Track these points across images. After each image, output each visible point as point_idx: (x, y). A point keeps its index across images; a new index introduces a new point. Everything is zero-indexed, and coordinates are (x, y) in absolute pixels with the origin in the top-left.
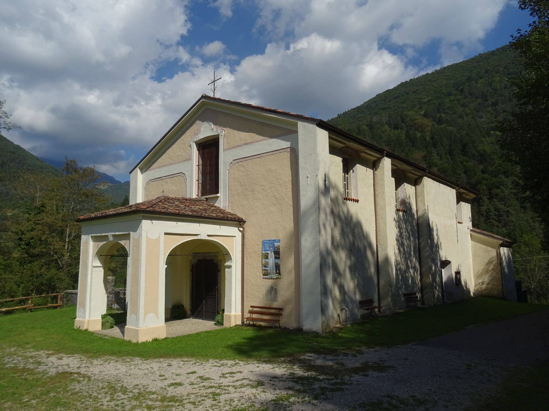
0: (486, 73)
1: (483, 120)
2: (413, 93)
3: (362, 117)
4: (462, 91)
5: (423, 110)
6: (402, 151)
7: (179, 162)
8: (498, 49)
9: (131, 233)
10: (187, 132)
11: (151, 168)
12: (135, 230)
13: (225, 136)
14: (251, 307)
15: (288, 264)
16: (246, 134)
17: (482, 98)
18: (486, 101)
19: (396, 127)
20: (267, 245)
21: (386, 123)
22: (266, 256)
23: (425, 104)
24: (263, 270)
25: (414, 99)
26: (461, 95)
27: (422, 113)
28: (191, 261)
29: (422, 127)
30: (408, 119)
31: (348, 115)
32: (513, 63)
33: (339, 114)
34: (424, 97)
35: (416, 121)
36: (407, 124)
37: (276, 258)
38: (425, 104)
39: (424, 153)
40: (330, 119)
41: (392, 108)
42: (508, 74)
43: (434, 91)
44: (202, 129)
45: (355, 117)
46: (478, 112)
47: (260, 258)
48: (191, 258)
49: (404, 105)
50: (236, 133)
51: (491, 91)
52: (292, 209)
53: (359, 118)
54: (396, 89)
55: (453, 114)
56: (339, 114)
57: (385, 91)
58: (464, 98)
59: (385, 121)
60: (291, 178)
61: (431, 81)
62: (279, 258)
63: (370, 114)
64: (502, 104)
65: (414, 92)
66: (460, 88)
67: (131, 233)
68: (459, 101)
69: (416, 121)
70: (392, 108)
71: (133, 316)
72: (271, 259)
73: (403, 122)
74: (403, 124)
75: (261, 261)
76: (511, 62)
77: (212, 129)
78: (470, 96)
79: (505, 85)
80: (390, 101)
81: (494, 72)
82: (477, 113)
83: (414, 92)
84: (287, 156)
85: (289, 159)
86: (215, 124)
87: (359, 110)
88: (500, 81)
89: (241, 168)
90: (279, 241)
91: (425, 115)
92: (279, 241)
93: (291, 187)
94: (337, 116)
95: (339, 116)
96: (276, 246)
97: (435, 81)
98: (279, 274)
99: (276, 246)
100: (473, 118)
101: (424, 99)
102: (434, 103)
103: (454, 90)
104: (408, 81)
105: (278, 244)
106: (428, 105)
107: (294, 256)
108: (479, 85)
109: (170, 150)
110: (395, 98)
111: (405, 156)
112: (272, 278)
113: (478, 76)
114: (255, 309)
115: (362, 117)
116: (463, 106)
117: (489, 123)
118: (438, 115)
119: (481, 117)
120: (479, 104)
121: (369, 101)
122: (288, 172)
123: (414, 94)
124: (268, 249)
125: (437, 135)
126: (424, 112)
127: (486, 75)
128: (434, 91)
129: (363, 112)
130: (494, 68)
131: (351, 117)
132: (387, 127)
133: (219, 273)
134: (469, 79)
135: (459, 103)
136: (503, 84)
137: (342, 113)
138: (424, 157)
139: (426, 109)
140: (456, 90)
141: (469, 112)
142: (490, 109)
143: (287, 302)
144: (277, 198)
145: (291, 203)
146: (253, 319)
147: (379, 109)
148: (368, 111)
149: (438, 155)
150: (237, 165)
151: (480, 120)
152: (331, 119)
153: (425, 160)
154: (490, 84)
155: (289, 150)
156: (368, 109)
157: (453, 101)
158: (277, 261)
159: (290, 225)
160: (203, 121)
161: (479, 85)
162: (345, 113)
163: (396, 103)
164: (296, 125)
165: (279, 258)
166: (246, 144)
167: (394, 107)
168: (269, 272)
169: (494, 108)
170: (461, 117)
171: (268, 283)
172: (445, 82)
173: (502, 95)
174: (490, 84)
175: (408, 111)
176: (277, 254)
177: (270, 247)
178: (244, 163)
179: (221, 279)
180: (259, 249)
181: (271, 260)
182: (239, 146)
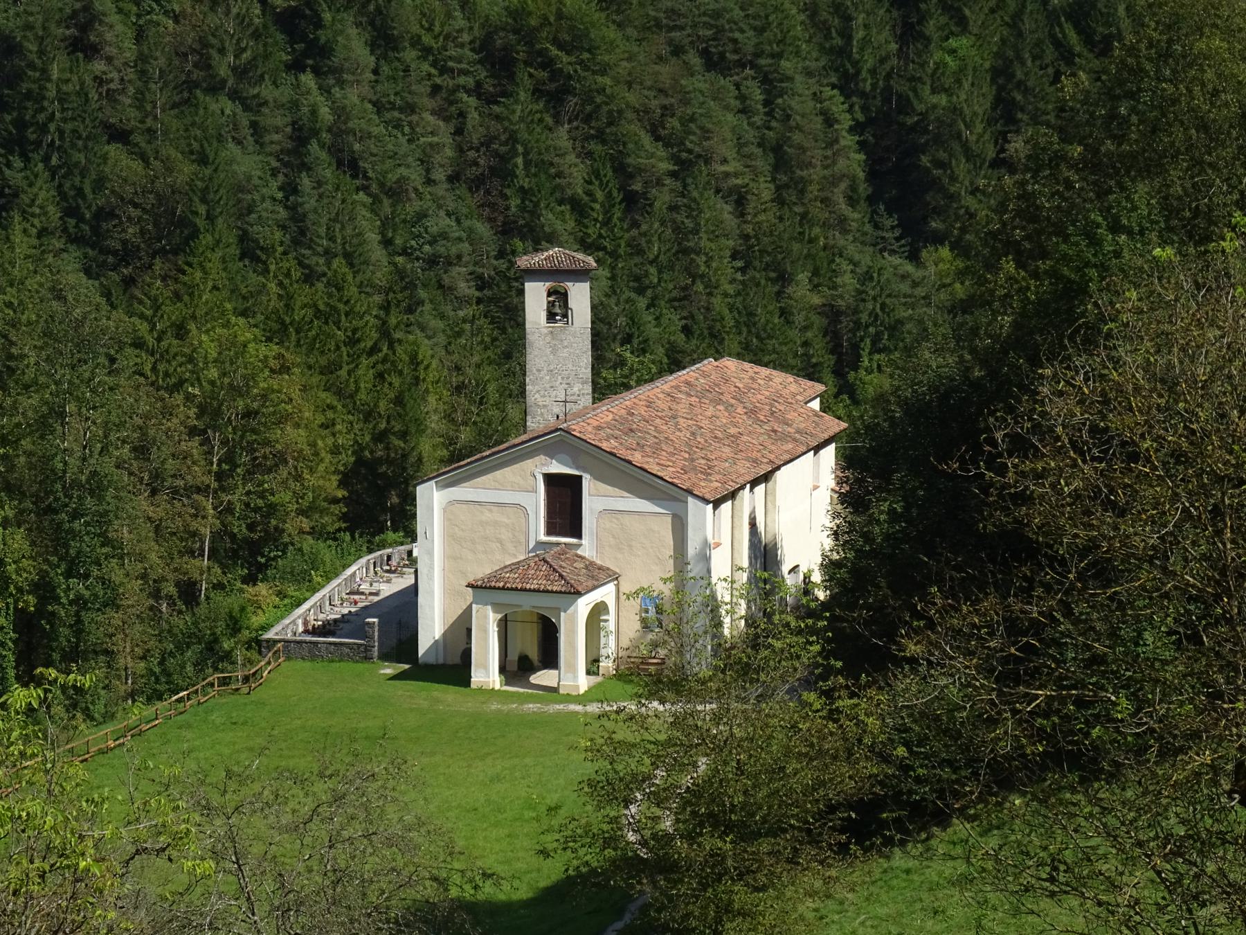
71: (570, 675)
159: (669, 569)
178: (619, 516)
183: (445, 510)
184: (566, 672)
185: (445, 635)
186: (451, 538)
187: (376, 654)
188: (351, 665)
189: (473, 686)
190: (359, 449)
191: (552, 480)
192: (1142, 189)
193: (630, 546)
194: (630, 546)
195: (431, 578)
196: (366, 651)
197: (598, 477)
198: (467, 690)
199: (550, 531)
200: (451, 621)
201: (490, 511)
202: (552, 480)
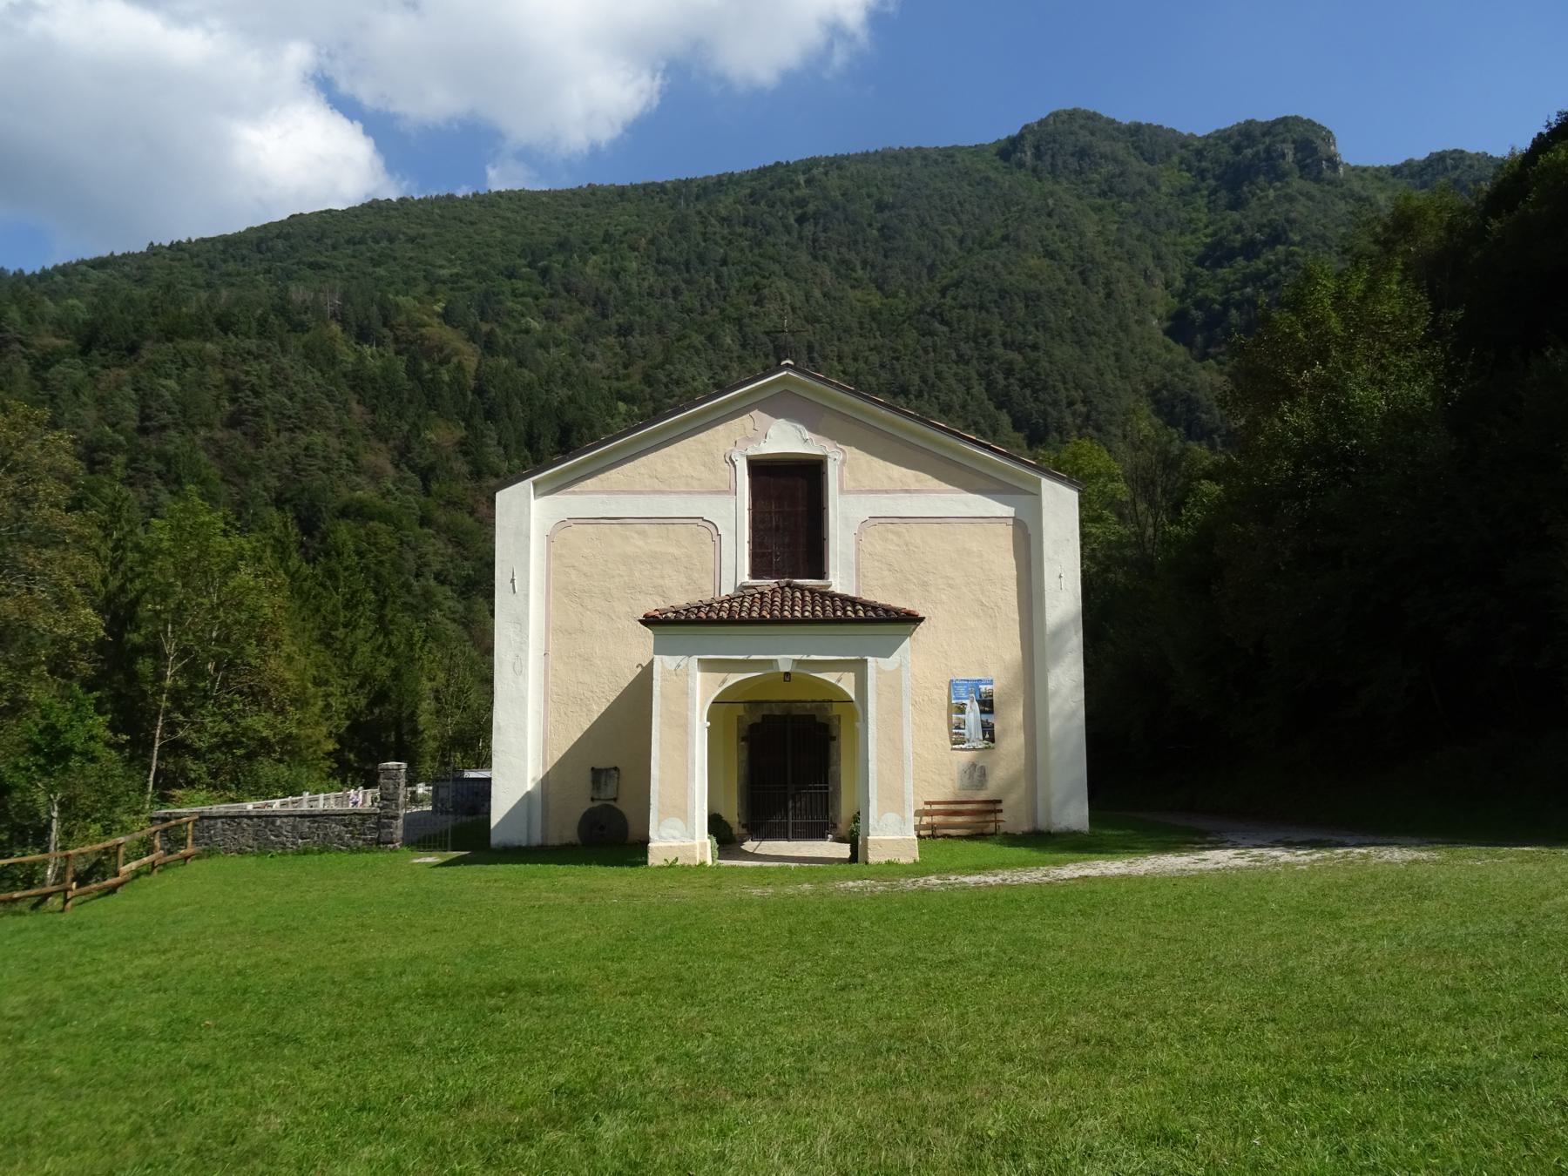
0: (604, 241)
1: (596, 365)
2: (407, 241)
3: (239, 274)
4: (545, 273)
5: (439, 300)
6: (400, 416)
7: (689, 493)
8: (635, 187)
9: (870, 659)
10: (720, 427)
11: (576, 488)
12: (887, 653)
13: (843, 462)
14: (926, 803)
15: (1011, 720)
16: (904, 470)
17: (594, 305)
18: (605, 316)
19: (363, 335)
20: (962, 691)
21: (334, 315)
22: (961, 709)
23: (444, 282)
24: (951, 734)
25: (411, 258)
26: (544, 285)
27: (438, 308)
28: (740, 719)
29: (441, 350)
30: (402, 318)
31: (187, 256)
32: (670, 237)
33: (156, 244)
34: (440, 262)
35: (424, 331)
36: (399, 333)
37: (982, 712)
38: (444, 282)
39: (460, 433)
40: (118, 253)
41: (341, 272)
42: (658, 261)
43: (469, 254)
44: (771, 433)
45: (212, 267)
46: (585, 342)
47: (945, 714)
48: (740, 710)
49: (381, 271)
50: (878, 463)
51: (618, 293)
52: (1017, 627)
53: (229, 275)
54: (356, 216)
55: (521, 332)
56: (156, 244)
57: (321, 212)
58: (551, 296)
59: (329, 309)
60: (1015, 572)
61: (461, 221)
62: (991, 712)
63: (268, 271)
64: (642, 335)
65: (412, 240)
66: (540, 264)
67: (870, 659)
68: (537, 298)
69: (424, 331)
70: (341, 272)
72: (972, 715)
73: (385, 325)
74: (386, 331)
75: (945, 716)
76: (666, 231)
77: (806, 441)
78: (565, 294)
79: (651, 287)
80: (334, 248)
81: (625, 245)
82: (582, 346)
83: (412, 240)
84: (1004, 538)
85: (1011, 538)
86: (812, 429)
87: (229, 245)
88: (639, 273)
89: (891, 536)
90: (991, 682)
91: (447, 317)
92: (991, 682)
93: (1015, 588)
94: (145, 250)
95: (154, 251)
96: (983, 690)
97: (472, 223)
98: (992, 740)
99: (983, 690)
100: (572, 355)
101: (441, 267)
102: (468, 288)
103: (525, 266)
104: (394, 200)
105: (989, 687)
106: (452, 289)
107: (1021, 710)
108: (588, 270)
109: (651, 456)
110: (350, 241)
111: (410, 431)
112: (974, 749)
113: (586, 243)
114: (935, 807)
115: (239, 274)
116: (548, 315)
117: (608, 378)
118: (485, 328)
119: (592, 358)
120: (588, 320)
121: (265, 226)
122: (1006, 566)
123: (410, 246)
124: (964, 695)
125: (494, 387)
126: (445, 308)
127: (606, 246)
128: (469, 254)
129: (243, 260)
130: (625, 233)
131: (199, 265)
132: (336, 328)
133: (834, 744)
134: (563, 245)
135: (537, 306)
136: (646, 284)
137: (167, 243)
138: (462, 443)
139: (450, 302)
140: (530, 265)
141: (563, 336)
142: (612, 340)
143: (1010, 786)
144: (982, 604)
145: (1017, 617)
146: (932, 827)
147: (298, 264)
148: (261, 260)
149: (499, 443)
150: (880, 527)
151: (588, 364)
152: (124, 256)
153: (466, 454)
154: (616, 275)
155: (1011, 522)
156: (260, 252)
157: (523, 295)
158: (985, 717)
159: (1011, 651)
160: (777, 416)
161: (588, 270)
162: (177, 247)
163: (354, 257)
164: (1039, 483)
165: (991, 712)
166: (907, 491)
167: (347, 270)
168: (967, 736)
169: (622, 339)
170: (543, 345)
171: (965, 757)
172: (499, 234)
173: (641, 312)
174: (616, 275)
175: (397, 293)
176: (987, 705)
177: (969, 692)
178: (902, 528)
179: (839, 755)
180: (941, 696)
181: (973, 715)
182: (887, 492)
183: (550, 539)
184: (882, 811)
185: (545, 782)
186: (562, 590)
187: (399, 833)
188: (346, 858)
189: (655, 859)
190: (351, 713)
191: (765, 472)
192: (1218, 330)
193: (925, 584)
194: (925, 584)
195: (520, 670)
196: (380, 826)
197: (852, 452)
198: (640, 869)
199: (755, 573)
200: (558, 755)
201: (643, 534)
202: (765, 472)
